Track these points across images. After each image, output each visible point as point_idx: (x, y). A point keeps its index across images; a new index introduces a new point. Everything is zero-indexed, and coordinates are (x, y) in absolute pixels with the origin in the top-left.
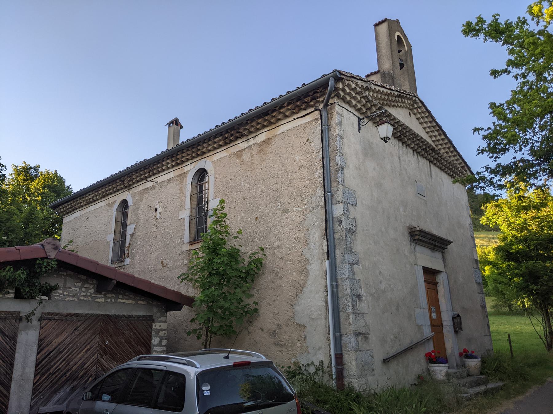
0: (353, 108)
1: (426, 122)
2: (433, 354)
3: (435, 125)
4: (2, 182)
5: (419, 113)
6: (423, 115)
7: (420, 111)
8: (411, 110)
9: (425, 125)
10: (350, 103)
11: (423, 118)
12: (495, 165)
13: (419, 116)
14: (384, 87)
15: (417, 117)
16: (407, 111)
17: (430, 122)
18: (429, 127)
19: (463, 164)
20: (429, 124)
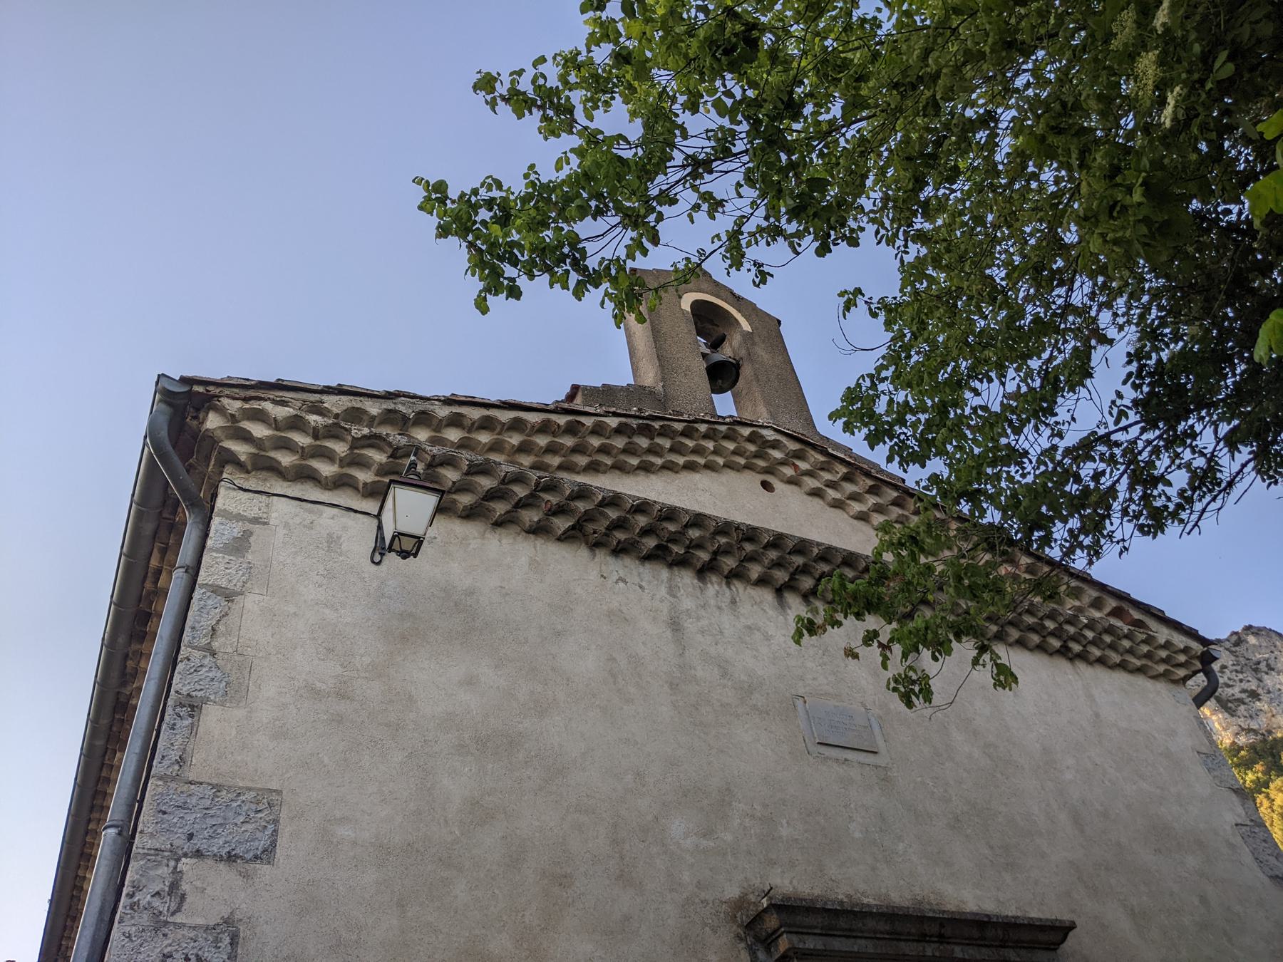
0: (747, 471)
1: (854, 497)
2: (811, 230)
3: (895, 494)
4: (1278, 375)
5: (810, 474)
6: (827, 476)
7: (803, 466)
8: (767, 471)
9: (856, 507)
10: (658, 449)
11: (832, 485)
12: (889, 631)
13: (811, 483)
14: (607, 414)
15: (807, 489)
16: (753, 479)
17: (873, 490)
18: (878, 509)
19: (1112, 603)
20: (872, 500)
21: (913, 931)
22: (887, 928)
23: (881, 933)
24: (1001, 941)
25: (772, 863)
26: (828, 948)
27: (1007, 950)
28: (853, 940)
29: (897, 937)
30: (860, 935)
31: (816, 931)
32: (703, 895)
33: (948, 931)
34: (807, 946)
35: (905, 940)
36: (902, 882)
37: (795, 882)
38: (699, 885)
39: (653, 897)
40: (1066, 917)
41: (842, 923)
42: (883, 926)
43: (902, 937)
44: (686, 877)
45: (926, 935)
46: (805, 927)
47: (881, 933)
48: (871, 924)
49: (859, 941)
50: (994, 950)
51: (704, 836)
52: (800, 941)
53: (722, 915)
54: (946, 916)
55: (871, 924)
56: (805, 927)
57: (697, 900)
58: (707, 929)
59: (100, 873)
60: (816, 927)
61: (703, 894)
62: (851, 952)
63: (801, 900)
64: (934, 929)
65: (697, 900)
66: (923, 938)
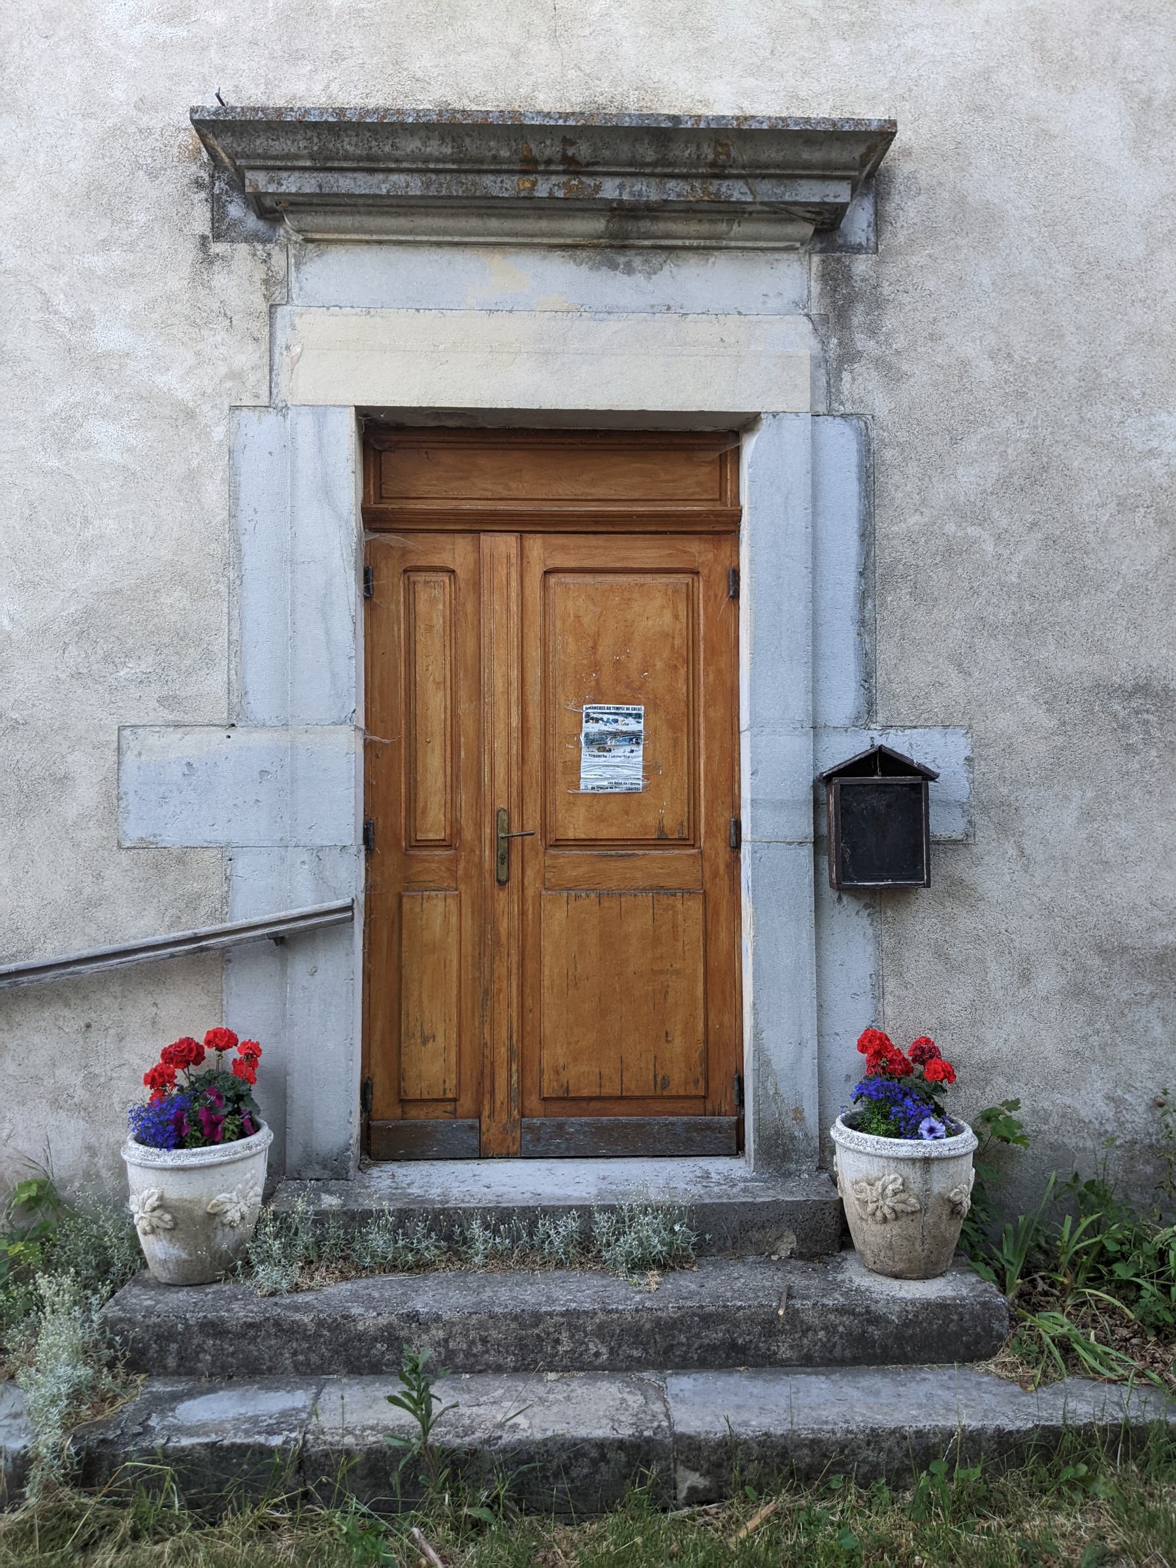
21: (505, 153)
22: (447, 150)
23: (438, 160)
24: (713, 165)
25: (295, 57)
26: (326, 190)
27: (726, 183)
28: (381, 176)
29: (476, 167)
30: (393, 165)
31: (301, 163)
32: (145, 121)
33: (583, 151)
34: (282, 189)
35: (492, 172)
36: (572, 74)
37: (334, 88)
38: (141, 105)
39: (51, 129)
40: (873, 114)
41: (349, 145)
42: (434, 148)
43: (485, 167)
44: (119, 93)
45: (536, 162)
46: (276, 158)
47: (438, 160)
48: (412, 145)
49: (394, 177)
50: (697, 184)
51: (170, 20)
52: (271, 181)
53: (175, 151)
54: (571, 122)
55: (412, 145)
56: (276, 158)
57: (132, 129)
58: (141, 173)
59: (579, 490)
60: (297, 157)
61: (146, 118)
62: (375, 196)
63: (255, 110)
64: (552, 149)
65: (132, 129)
66: (530, 166)
